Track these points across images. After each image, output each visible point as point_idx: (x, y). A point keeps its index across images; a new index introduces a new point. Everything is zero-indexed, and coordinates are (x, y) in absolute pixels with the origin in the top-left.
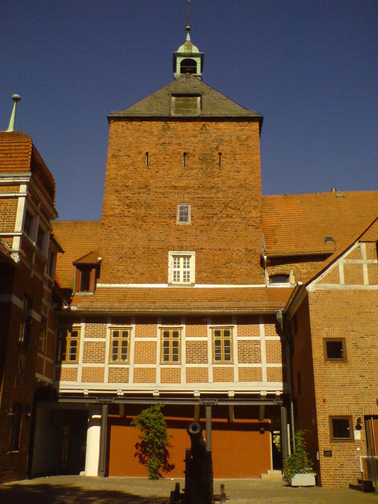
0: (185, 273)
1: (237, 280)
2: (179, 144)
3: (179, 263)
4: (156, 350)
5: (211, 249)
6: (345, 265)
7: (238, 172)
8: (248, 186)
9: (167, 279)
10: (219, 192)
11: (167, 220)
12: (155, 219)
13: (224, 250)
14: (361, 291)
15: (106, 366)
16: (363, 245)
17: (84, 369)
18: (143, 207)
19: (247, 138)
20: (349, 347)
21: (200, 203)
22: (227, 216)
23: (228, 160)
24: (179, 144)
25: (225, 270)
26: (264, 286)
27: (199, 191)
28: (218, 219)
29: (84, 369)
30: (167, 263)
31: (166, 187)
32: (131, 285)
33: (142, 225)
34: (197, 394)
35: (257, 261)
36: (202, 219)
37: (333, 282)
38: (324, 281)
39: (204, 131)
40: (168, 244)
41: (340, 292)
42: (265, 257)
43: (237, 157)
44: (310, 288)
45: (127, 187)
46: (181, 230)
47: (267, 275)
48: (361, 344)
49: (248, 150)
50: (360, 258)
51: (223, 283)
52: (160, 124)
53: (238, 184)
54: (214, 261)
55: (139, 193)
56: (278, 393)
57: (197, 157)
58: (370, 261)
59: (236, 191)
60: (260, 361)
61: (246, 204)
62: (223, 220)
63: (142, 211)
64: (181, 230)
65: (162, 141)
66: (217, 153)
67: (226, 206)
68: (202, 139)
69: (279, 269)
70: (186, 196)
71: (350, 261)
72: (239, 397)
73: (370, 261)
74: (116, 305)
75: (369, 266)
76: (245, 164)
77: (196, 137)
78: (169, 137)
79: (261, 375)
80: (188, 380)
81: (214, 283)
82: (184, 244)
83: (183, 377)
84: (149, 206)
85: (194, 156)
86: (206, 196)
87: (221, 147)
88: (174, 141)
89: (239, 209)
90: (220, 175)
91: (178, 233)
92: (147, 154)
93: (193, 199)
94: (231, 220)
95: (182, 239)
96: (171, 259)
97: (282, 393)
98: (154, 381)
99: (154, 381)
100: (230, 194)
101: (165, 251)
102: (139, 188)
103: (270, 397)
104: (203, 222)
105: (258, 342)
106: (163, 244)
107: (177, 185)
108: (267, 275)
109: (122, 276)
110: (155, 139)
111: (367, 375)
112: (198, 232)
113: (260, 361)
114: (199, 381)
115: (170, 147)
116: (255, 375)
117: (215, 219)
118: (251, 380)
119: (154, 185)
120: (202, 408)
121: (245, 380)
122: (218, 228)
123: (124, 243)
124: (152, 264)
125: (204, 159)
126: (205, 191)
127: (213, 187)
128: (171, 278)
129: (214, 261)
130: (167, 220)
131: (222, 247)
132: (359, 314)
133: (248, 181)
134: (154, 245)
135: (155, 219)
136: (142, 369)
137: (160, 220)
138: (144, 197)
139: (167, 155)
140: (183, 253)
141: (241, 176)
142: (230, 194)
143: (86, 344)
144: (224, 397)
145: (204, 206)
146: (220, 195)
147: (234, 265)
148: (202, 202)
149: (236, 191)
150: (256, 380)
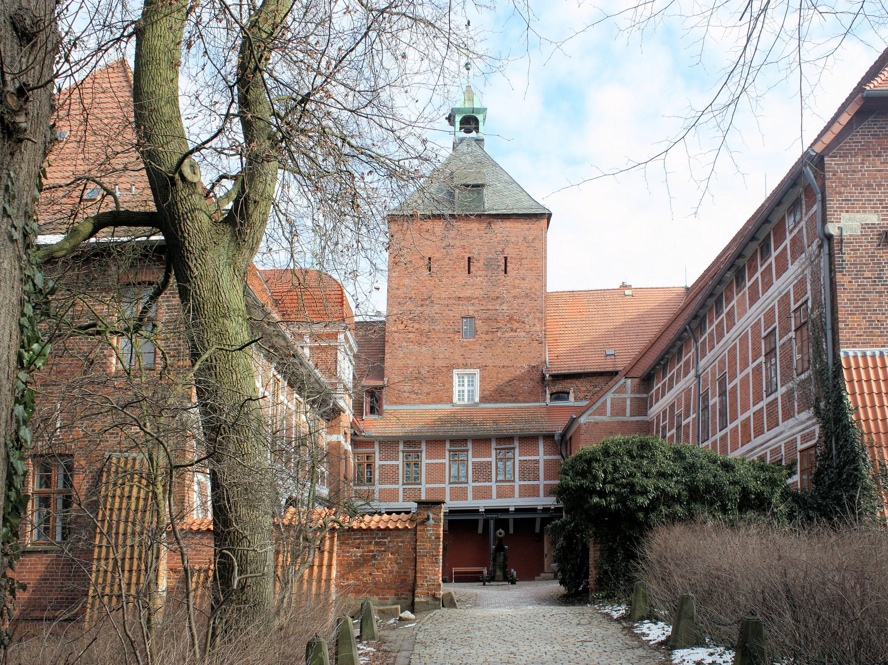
0: (463, 385)
1: (520, 398)
2: (464, 247)
3: (463, 381)
4: (445, 470)
5: (495, 366)
6: (612, 399)
7: (523, 279)
8: (533, 296)
9: (452, 399)
10: (504, 303)
11: (452, 336)
12: (439, 335)
13: (508, 367)
14: (623, 422)
15: (518, 483)
16: (629, 381)
18: (427, 322)
19: (534, 239)
21: (485, 316)
22: (512, 330)
23: (513, 266)
24: (464, 247)
27: (484, 303)
28: (503, 333)
30: (452, 383)
31: (450, 298)
32: (416, 407)
33: (426, 342)
36: (487, 334)
38: (593, 414)
40: (452, 362)
41: (606, 423)
42: (547, 375)
43: (524, 261)
45: (410, 298)
46: (466, 346)
47: (548, 392)
49: (534, 254)
50: (625, 392)
54: (498, 378)
56: (553, 507)
57: (482, 261)
62: (507, 335)
63: (426, 327)
64: (466, 346)
66: (502, 256)
67: (510, 319)
69: (559, 387)
70: (470, 308)
71: (617, 395)
72: (518, 510)
73: (632, 396)
76: (531, 270)
79: (538, 491)
80: (475, 497)
81: (497, 401)
82: (469, 361)
84: (433, 321)
85: (478, 261)
86: (490, 307)
87: (507, 251)
89: (523, 322)
90: (505, 282)
91: (463, 349)
92: (430, 259)
93: (478, 311)
95: (466, 356)
96: (456, 379)
101: (450, 368)
102: (422, 301)
103: (546, 510)
104: (487, 337)
105: (537, 462)
106: (448, 362)
108: (548, 392)
109: (408, 397)
112: (482, 348)
114: (483, 498)
116: (533, 491)
117: (499, 334)
118: (529, 496)
119: (438, 296)
120: (486, 522)
122: (503, 343)
123: (409, 362)
124: (437, 384)
126: (490, 301)
127: (498, 297)
128: (455, 399)
130: (452, 336)
131: (506, 364)
133: (533, 290)
134: (439, 363)
135: (439, 335)
136: (433, 489)
138: (427, 311)
139: (450, 260)
140: (468, 371)
141: (525, 284)
143: (381, 466)
144: (505, 511)
148: (487, 315)
149: (520, 301)
150: (534, 496)
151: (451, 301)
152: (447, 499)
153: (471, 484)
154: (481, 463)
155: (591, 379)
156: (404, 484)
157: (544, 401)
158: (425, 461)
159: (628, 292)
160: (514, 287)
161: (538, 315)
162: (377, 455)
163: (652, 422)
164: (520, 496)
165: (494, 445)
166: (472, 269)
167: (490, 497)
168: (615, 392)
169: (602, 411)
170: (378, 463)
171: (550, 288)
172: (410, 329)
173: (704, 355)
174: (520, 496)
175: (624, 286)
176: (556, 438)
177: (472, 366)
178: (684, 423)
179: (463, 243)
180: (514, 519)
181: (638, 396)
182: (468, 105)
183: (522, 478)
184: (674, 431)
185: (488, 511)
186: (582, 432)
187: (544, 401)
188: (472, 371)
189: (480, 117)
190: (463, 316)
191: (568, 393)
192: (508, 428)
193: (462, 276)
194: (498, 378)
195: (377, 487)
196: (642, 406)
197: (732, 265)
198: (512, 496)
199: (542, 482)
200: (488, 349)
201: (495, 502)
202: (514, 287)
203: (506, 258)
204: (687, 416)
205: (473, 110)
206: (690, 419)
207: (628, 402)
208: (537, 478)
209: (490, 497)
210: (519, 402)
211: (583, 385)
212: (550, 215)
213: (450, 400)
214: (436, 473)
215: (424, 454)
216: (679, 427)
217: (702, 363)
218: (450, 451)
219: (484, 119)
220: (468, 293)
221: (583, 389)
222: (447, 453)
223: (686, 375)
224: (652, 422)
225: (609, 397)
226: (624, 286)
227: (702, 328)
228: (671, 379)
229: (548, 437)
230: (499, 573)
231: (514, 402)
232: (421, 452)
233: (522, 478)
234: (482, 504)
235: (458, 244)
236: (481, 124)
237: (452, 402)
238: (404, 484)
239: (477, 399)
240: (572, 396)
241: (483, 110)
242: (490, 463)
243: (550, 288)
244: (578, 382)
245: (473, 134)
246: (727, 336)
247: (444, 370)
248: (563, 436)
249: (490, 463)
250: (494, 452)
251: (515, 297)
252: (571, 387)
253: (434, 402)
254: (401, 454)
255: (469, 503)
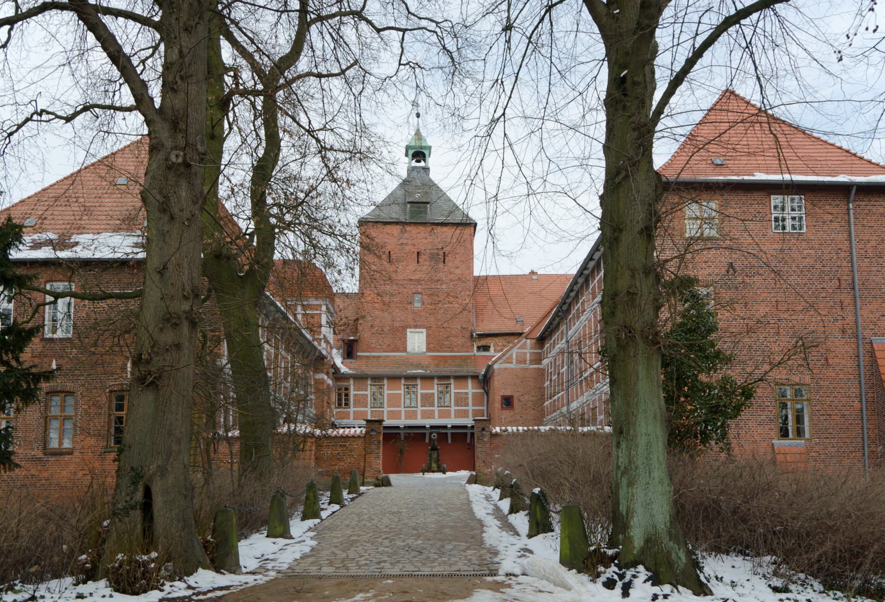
2: (414, 245)
6: (517, 353)
7: (457, 268)
16: (529, 341)
17: (354, 412)
20: (516, 402)
21: (430, 292)
22: (449, 303)
24: (414, 245)
25: (446, 343)
26: (472, 354)
28: (443, 305)
29: (354, 412)
34: (428, 426)
35: (468, 335)
37: (508, 363)
39: (432, 233)
40: (406, 324)
41: (513, 369)
44: (496, 366)
47: (475, 346)
48: (522, 399)
50: (526, 348)
51: (445, 352)
52: (399, 227)
53: (457, 278)
55: (385, 285)
58: (531, 351)
59: (455, 283)
60: (468, 406)
61: (463, 293)
62: (445, 306)
65: (401, 241)
68: (431, 240)
69: (483, 342)
71: (520, 351)
72: (453, 427)
73: (531, 351)
74: (374, 370)
75: (531, 353)
77: (426, 238)
78: (406, 239)
79: (468, 414)
80: (423, 417)
81: (438, 351)
82: (419, 323)
83: (419, 416)
85: (424, 255)
86: (434, 287)
88: (410, 242)
89: (457, 298)
93: (424, 289)
94: (451, 305)
96: (408, 334)
97: (186, 578)
98: (400, 418)
99: (400, 418)
100: (451, 286)
101: (405, 328)
104: (432, 307)
105: (467, 394)
107: (412, 278)
110: (396, 240)
111: (524, 417)
112: (428, 315)
113: (468, 406)
114: (429, 418)
115: (407, 248)
116: (465, 414)
118: (462, 417)
121: (458, 417)
125: (433, 257)
128: (409, 349)
129: (439, 335)
132: (522, 382)
134: (397, 324)
135: (397, 305)
136: (392, 411)
137: (400, 305)
142: (451, 286)
143: (355, 395)
144: (445, 427)
145: (432, 294)
146: (444, 286)
147: (453, 339)
149: (455, 283)
150: (465, 417)
151: (404, 282)
152: (385, 419)
153: (420, 409)
154: (427, 394)
155: (505, 337)
156: (371, 407)
157: (473, 352)
158: (386, 392)
159: (534, 277)
160: (451, 273)
161: (468, 293)
162: (352, 388)
163: (544, 370)
164: (455, 417)
165: (436, 381)
166: (420, 260)
167: (434, 418)
168: (519, 348)
169: (508, 360)
170: (352, 393)
171: (479, 270)
172: (376, 301)
173: (570, 329)
174: (455, 417)
175: (533, 273)
176: (480, 378)
177: (420, 327)
178: (561, 371)
179: (413, 242)
180: (452, 433)
181: (535, 351)
182: (418, 144)
183: (457, 404)
184: (556, 376)
185: (432, 427)
186: (495, 374)
187: (473, 352)
188: (421, 330)
189: (426, 152)
190: (414, 291)
191: (490, 347)
192: (445, 370)
193: (413, 265)
194: (439, 335)
195: (352, 409)
196: (538, 359)
197: (582, 274)
198: (449, 417)
199: (470, 408)
200: (432, 316)
201: (437, 421)
202: (451, 273)
203: (444, 253)
204: (563, 367)
205: (421, 147)
206: (564, 369)
207: (528, 355)
208: (467, 405)
209: (434, 418)
210: (454, 352)
211: (500, 341)
212: (476, 225)
213: (405, 350)
214: (394, 401)
215: (386, 387)
216: (559, 374)
217: (570, 333)
218: (404, 385)
219: (430, 154)
220: (417, 277)
221: (501, 344)
222: (403, 387)
223: (562, 339)
224: (544, 370)
225: (514, 352)
226: (533, 273)
227: (568, 311)
228: (554, 341)
229: (475, 377)
230: (434, 465)
231: (451, 352)
232: (384, 385)
233: (457, 404)
234: (428, 423)
235: (410, 242)
236: (427, 156)
237: (406, 351)
238: (371, 407)
239: (424, 350)
240: (492, 349)
241: (430, 148)
242: (433, 394)
243: (479, 270)
244: (496, 339)
245: (422, 164)
246: (582, 318)
247: (401, 329)
248: (485, 376)
249: (433, 394)
250: (436, 386)
251: (451, 280)
252: (491, 342)
253: (394, 351)
254: (369, 387)
255: (419, 421)
